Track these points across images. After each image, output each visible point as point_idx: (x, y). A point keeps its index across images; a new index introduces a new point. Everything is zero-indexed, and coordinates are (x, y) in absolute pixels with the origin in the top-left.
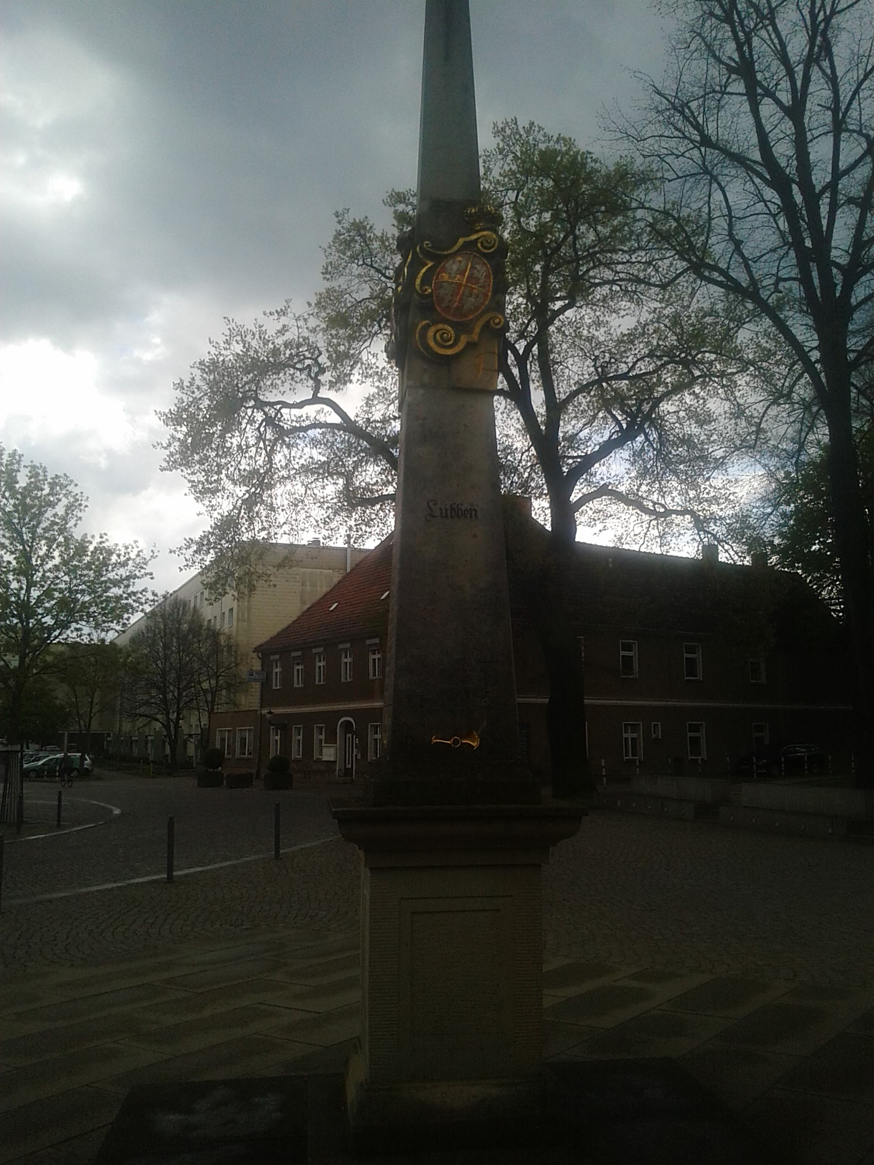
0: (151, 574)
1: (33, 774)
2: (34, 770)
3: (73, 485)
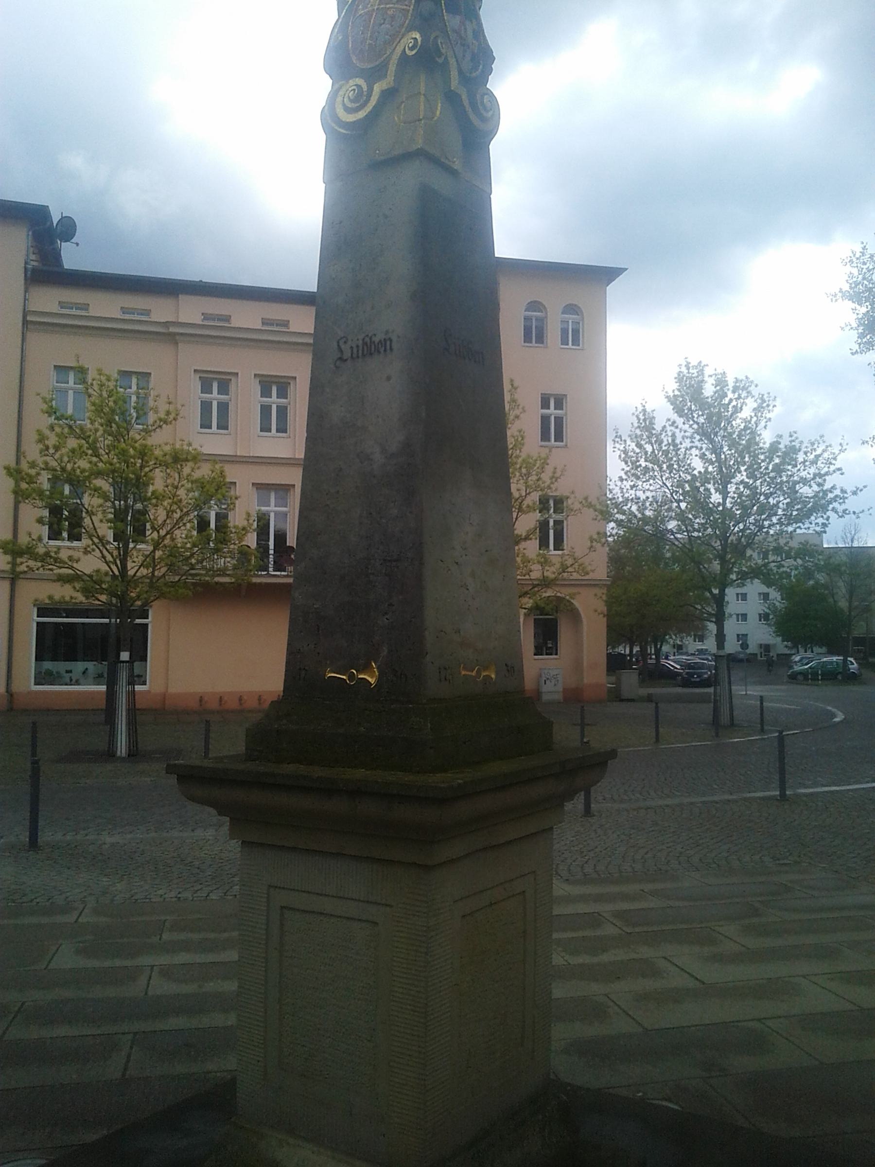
0: (839, 469)
1: (800, 677)
2: (800, 673)
3: (753, 386)
